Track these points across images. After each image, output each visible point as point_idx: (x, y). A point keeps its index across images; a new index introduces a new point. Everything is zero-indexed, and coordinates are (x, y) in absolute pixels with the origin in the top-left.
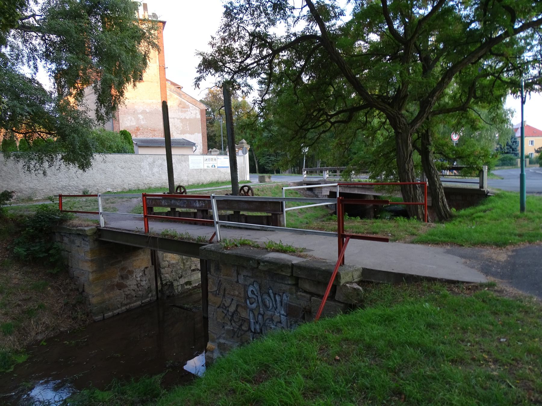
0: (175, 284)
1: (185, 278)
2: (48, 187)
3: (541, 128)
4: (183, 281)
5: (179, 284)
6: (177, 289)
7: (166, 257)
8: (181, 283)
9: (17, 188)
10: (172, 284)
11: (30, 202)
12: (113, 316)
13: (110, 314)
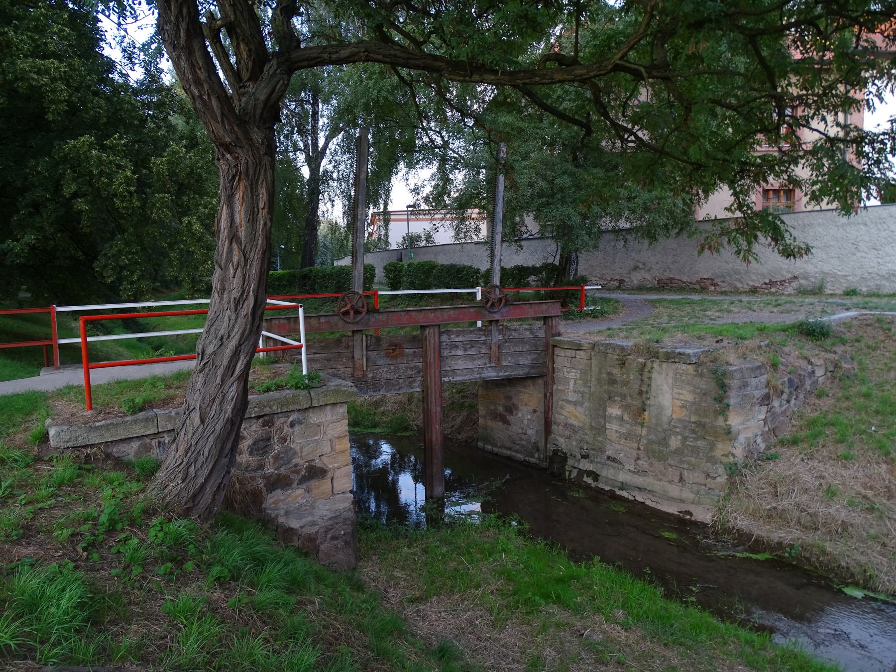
0: (570, 462)
1: (592, 462)
2: (859, 272)
3: (893, 578)
4: (585, 465)
5: (576, 465)
6: (570, 472)
7: (561, 408)
8: (581, 466)
9: (801, 271)
10: (565, 458)
11: (854, 297)
12: (491, 453)
13: (489, 447)
